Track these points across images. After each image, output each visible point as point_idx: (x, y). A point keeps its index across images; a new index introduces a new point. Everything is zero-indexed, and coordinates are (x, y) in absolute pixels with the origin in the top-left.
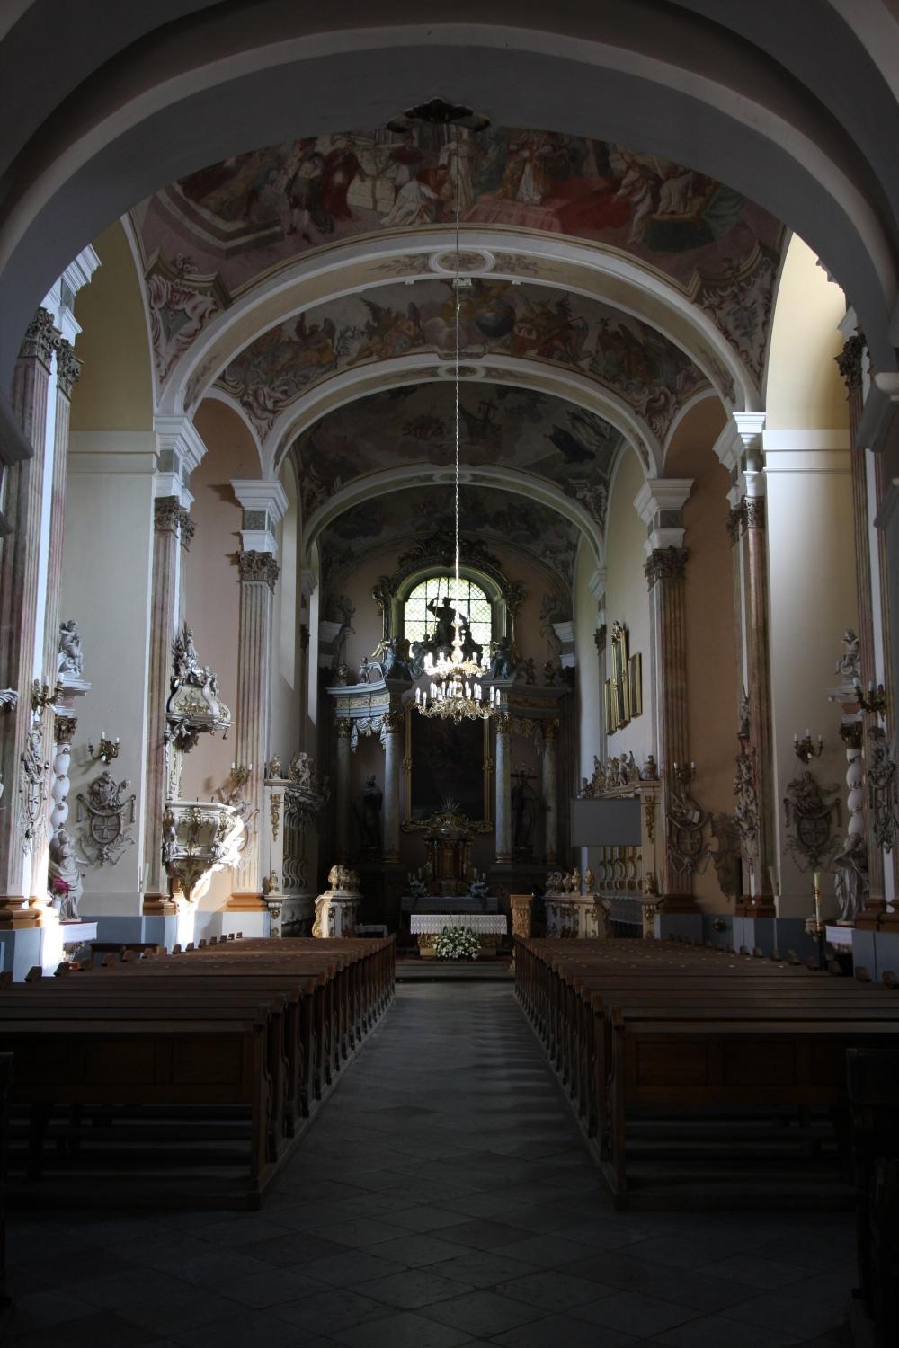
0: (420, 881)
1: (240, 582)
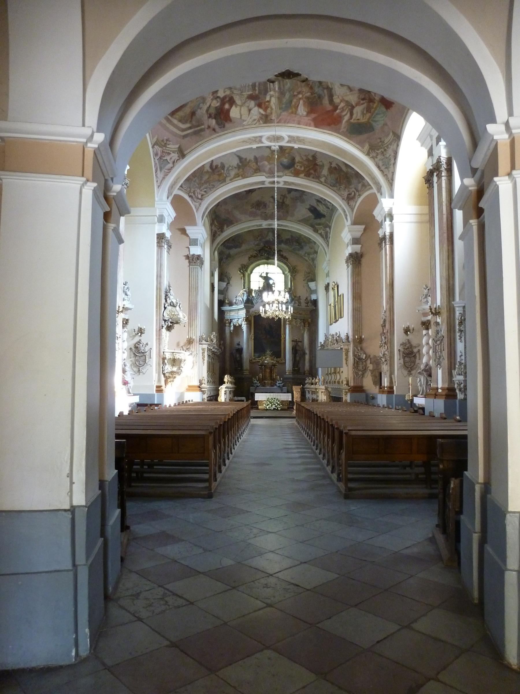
1: (189, 266)
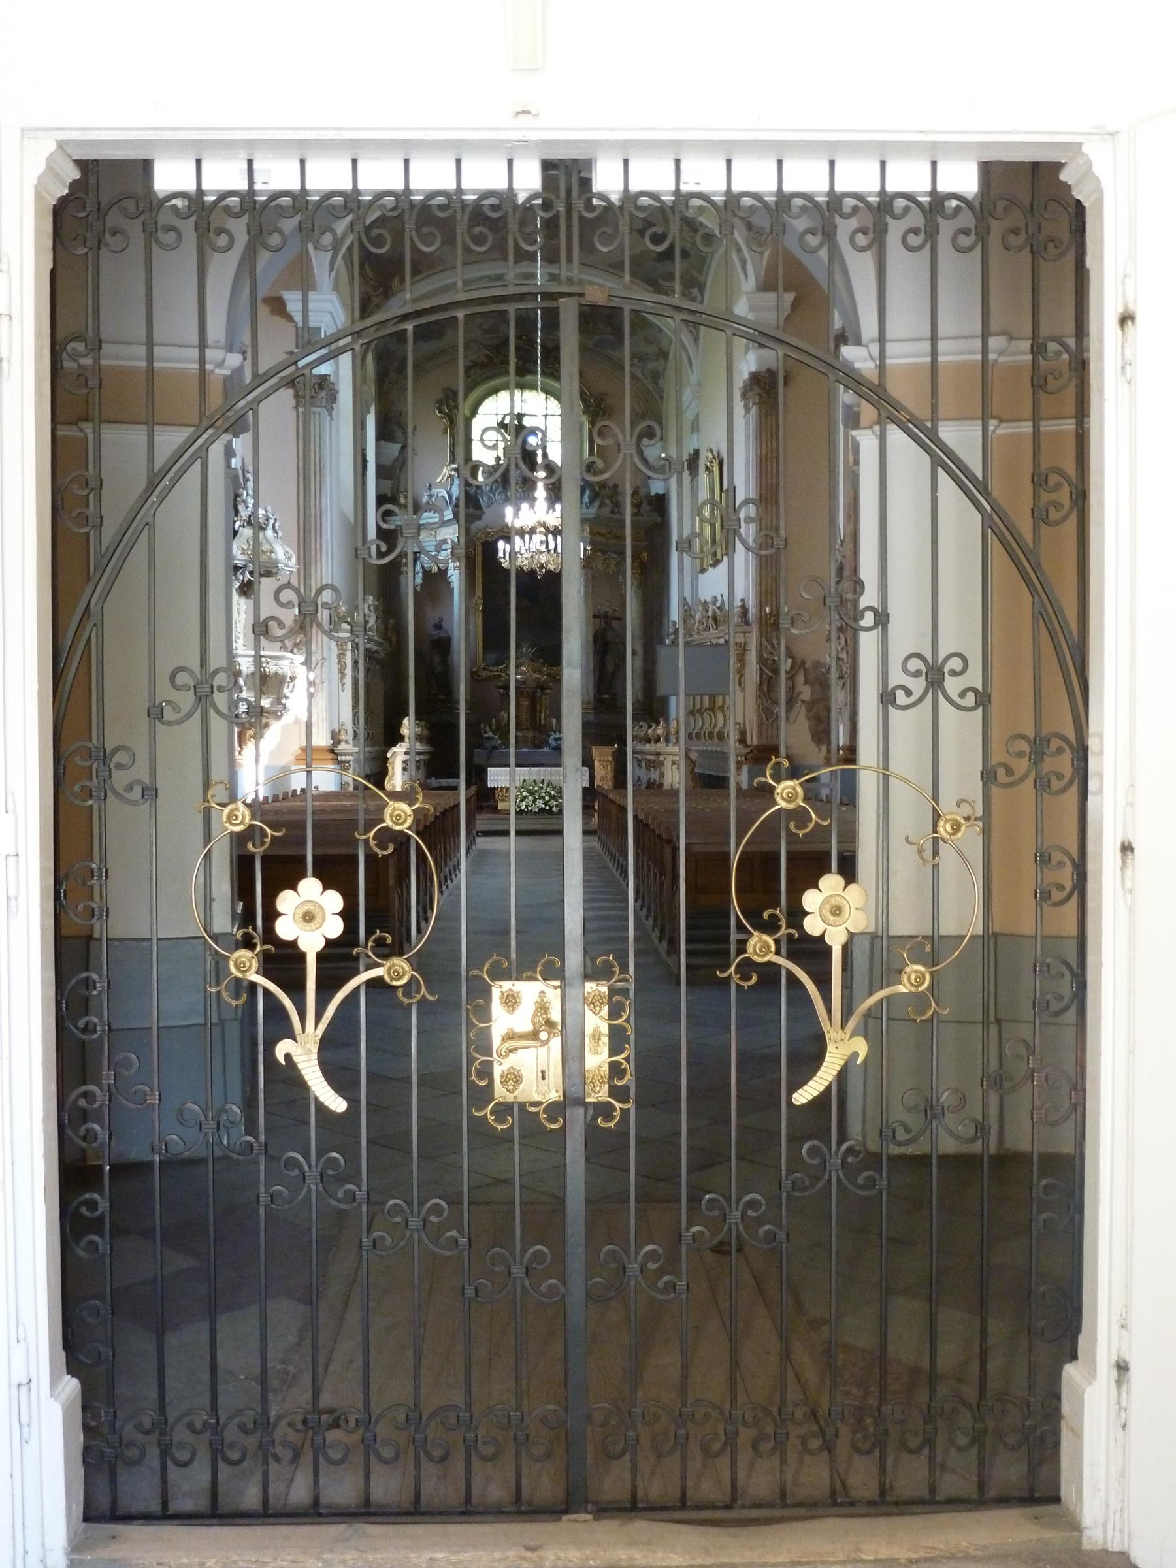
0: (494, 732)
1: (296, 408)
